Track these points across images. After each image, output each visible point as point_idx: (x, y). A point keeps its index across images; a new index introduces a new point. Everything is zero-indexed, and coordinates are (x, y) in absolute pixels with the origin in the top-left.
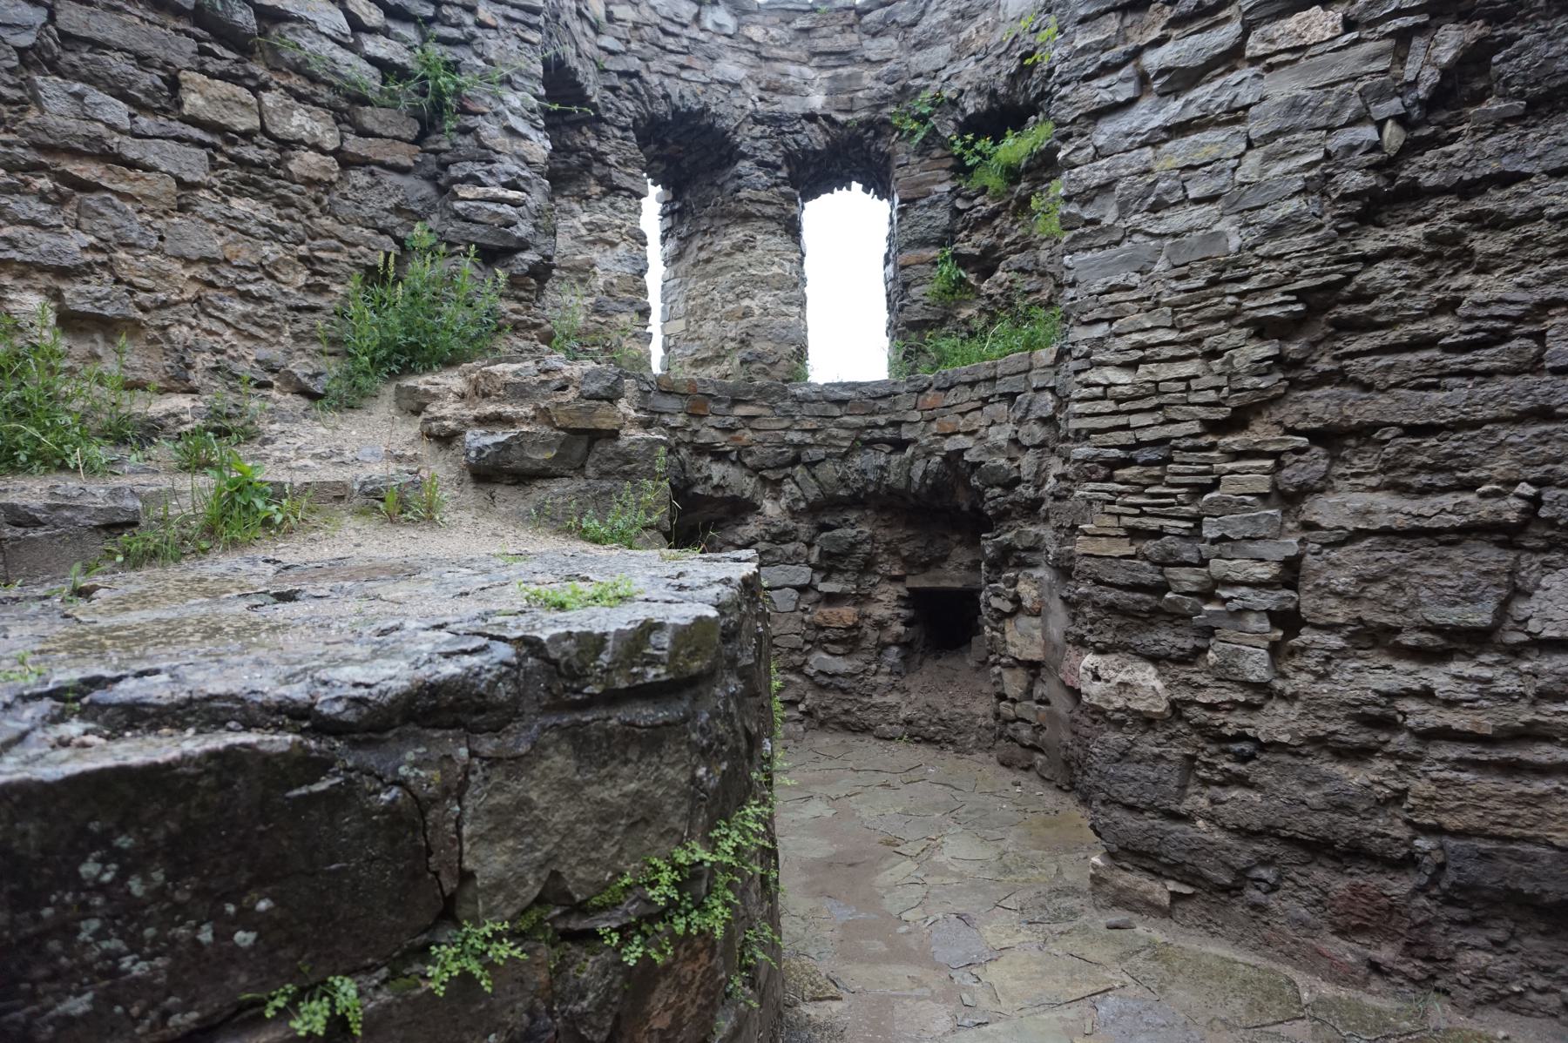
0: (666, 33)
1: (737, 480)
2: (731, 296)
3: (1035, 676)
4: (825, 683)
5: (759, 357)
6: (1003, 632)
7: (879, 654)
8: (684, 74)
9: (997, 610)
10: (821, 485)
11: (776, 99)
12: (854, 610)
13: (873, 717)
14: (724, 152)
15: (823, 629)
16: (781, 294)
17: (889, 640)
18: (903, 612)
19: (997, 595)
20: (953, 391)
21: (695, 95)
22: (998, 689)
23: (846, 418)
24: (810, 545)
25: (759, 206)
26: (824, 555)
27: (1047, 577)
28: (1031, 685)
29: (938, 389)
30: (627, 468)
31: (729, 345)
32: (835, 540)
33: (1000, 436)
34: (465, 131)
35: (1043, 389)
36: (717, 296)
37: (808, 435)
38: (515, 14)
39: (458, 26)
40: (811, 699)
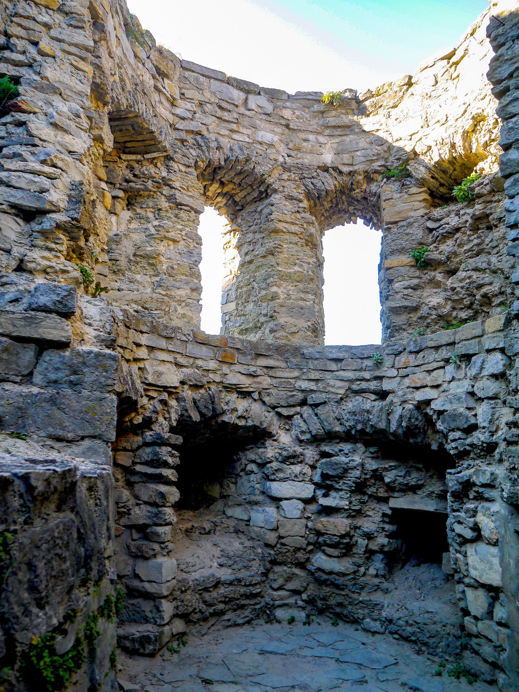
0: (220, 107)
1: (258, 413)
2: (264, 285)
3: (495, 598)
4: (322, 579)
5: (283, 327)
6: (465, 556)
7: (368, 559)
8: (235, 136)
9: (460, 536)
10: (321, 423)
11: (299, 156)
12: (347, 521)
13: (360, 612)
14: (262, 189)
15: (323, 534)
16: (301, 286)
17: (376, 548)
18: (387, 527)
19: (460, 523)
20: (421, 355)
21: (241, 150)
22: (462, 604)
23: (341, 373)
24: (313, 467)
25: (284, 225)
26: (324, 476)
27: (503, 511)
28: (491, 606)
29: (411, 352)
30: (72, 378)
31: (262, 319)
32: (332, 464)
33: (460, 388)
34: (21, 124)
35: (494, 350)
36: (256, 286)
37: (313, 383)
38: (73, 49)
39: (24, 53)
40: (313, 590)
